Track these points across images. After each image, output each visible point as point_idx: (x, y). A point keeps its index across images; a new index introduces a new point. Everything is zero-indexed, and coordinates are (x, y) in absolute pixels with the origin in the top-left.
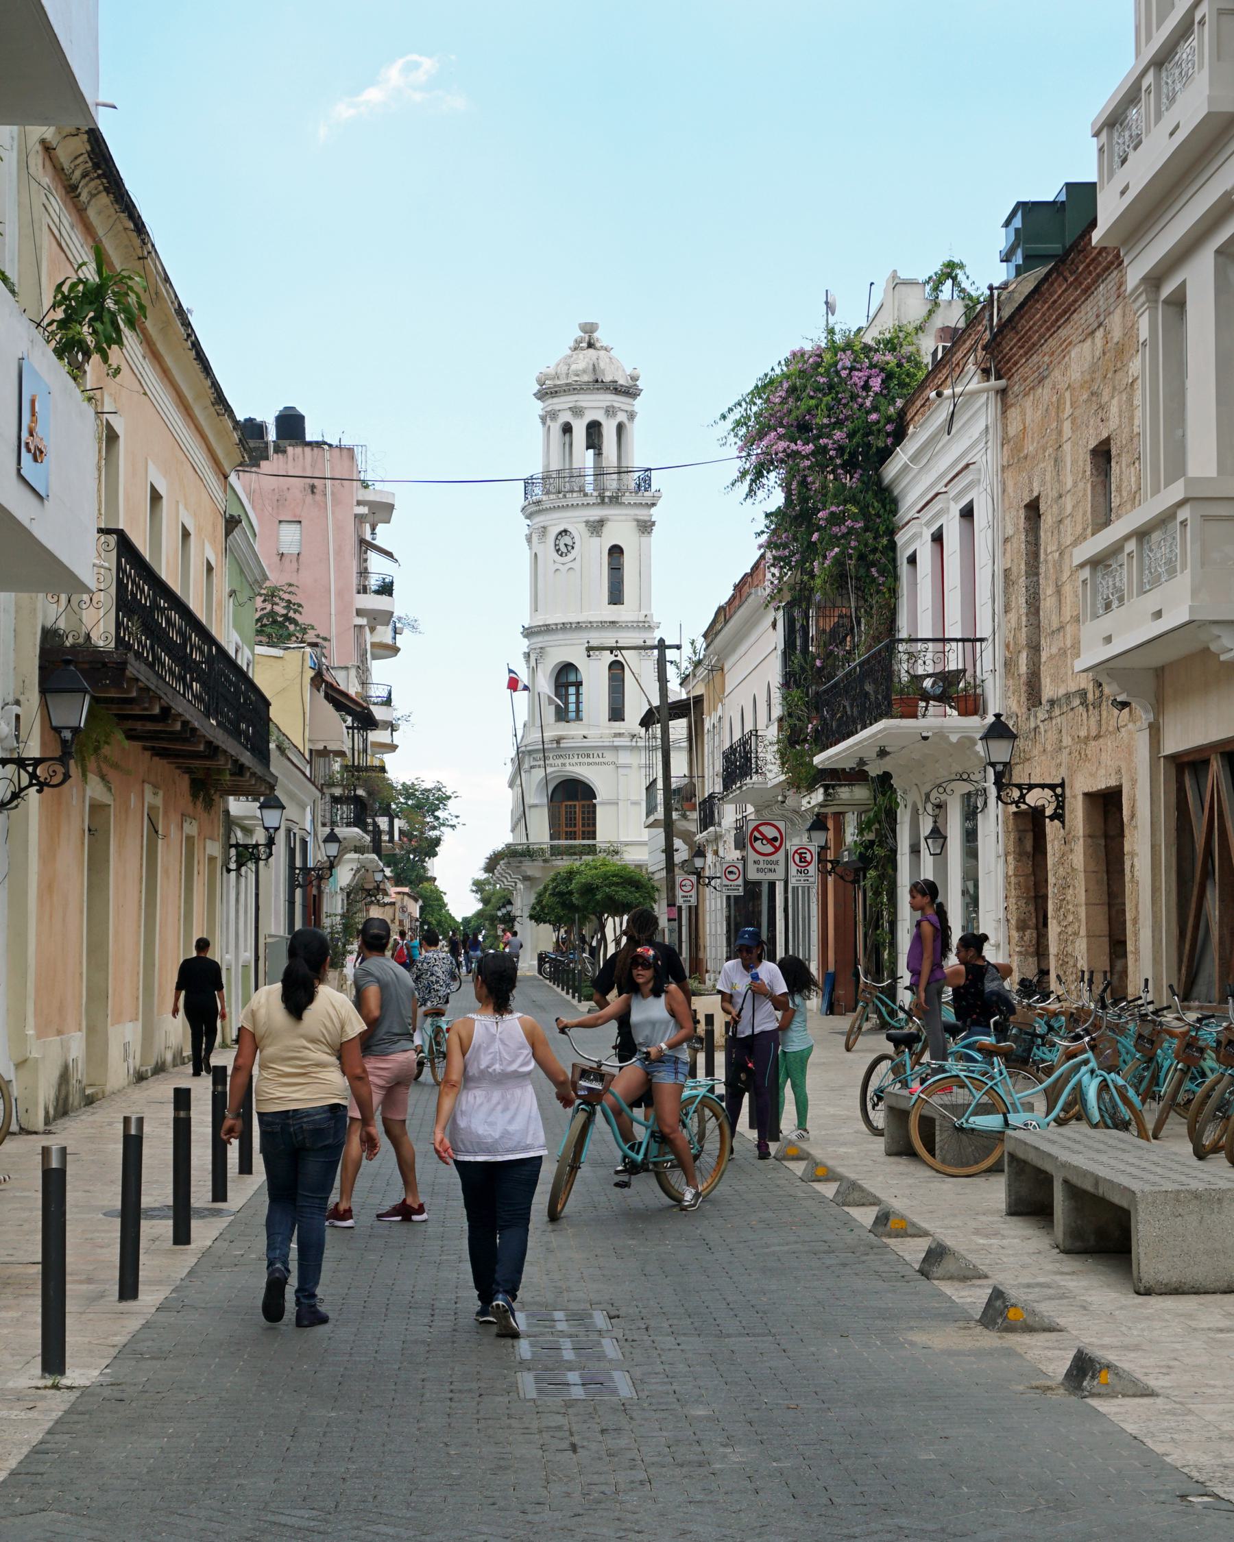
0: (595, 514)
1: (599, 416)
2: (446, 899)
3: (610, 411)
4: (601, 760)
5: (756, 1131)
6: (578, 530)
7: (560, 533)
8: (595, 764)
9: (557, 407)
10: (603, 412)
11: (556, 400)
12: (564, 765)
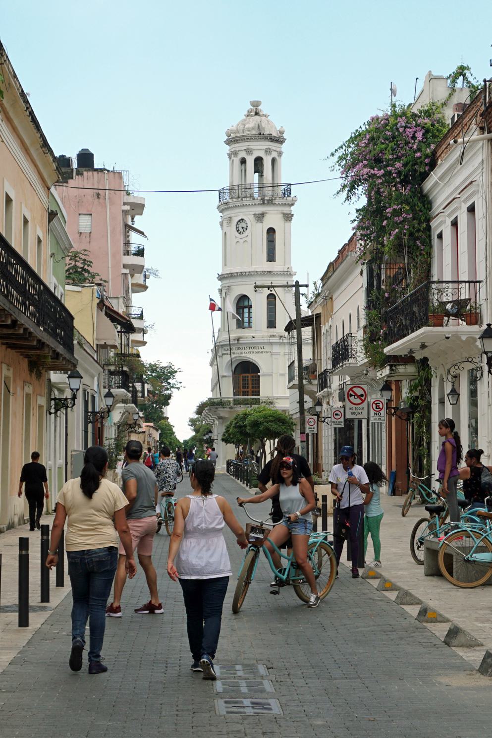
0: (259, 210)
1: (261, 154)
2: (174, 430)
3: (268, 151)
4: (263, 350)
5: (58, 156)
6: (250, 219)
7: (239, 221)
8: (259, 352)
9: (238, 149)
10: (264, 151)
11: (237, 145)
12: (241, 353)
